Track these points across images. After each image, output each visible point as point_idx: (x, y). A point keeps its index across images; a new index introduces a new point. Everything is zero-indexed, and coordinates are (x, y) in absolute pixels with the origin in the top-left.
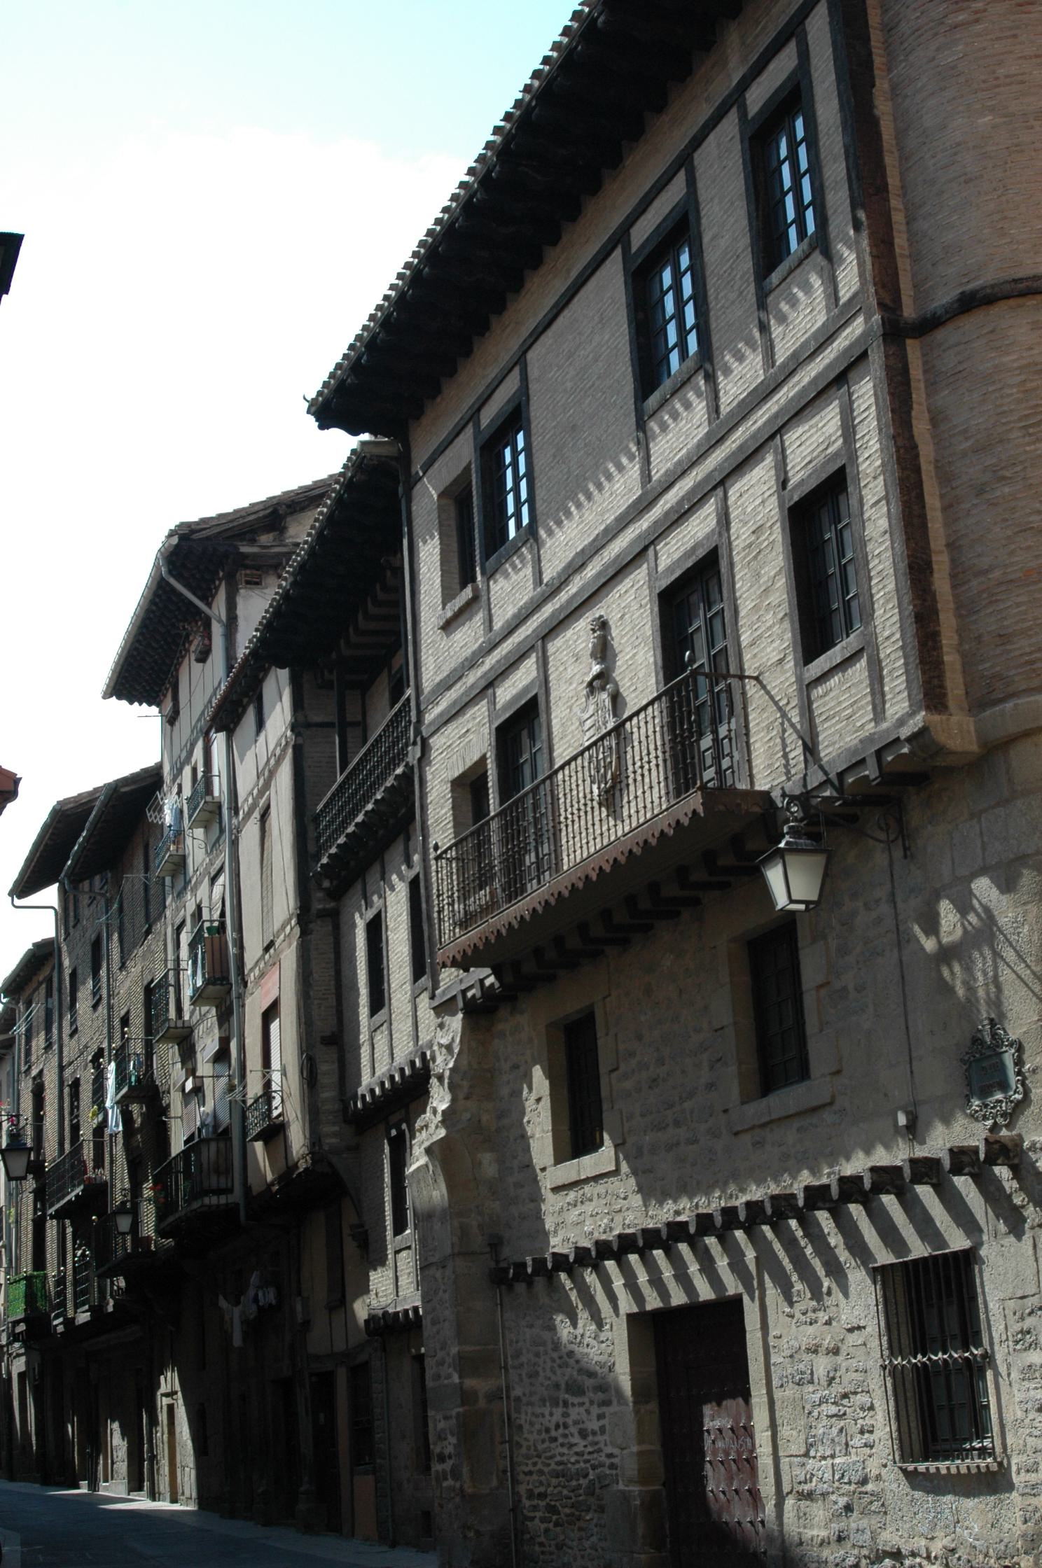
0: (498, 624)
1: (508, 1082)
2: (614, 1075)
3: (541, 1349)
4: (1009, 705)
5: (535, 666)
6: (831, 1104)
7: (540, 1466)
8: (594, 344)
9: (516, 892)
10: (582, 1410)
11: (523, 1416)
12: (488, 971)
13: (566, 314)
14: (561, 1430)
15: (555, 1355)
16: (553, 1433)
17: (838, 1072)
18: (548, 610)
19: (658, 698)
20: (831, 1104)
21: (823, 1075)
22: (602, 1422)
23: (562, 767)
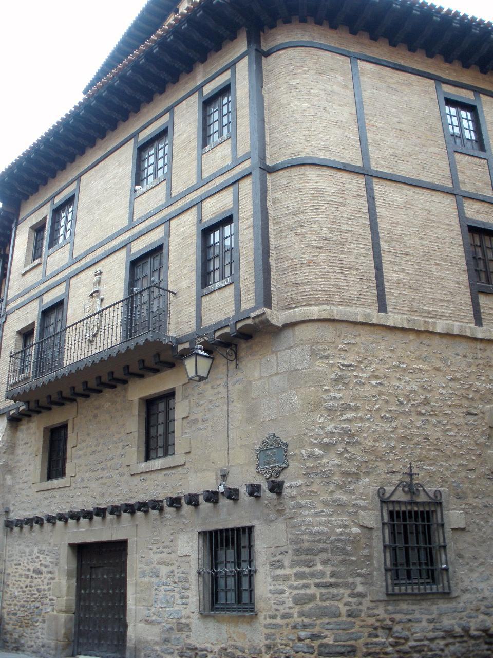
0: (48, 273)
1: (22, 449)
2: (74, 449)
3: (23, 554)
4: (298, 310)
5: (64, 288)
6: (184, 465)
7: (15, 602)
8: (114, 173)
9: (42, 372)
10: (40, 581)
11: (10, 581)
12: (22, 403)
13: (103, 163)
14: (28, 588)
15: (30, 558)
16: (25, 589)
17: (189, 453)
18: (74, 267)
19: (122, 301)
20: (184, 465)
21: (182, 453)
22: (49, 586)
23: (69, 327)
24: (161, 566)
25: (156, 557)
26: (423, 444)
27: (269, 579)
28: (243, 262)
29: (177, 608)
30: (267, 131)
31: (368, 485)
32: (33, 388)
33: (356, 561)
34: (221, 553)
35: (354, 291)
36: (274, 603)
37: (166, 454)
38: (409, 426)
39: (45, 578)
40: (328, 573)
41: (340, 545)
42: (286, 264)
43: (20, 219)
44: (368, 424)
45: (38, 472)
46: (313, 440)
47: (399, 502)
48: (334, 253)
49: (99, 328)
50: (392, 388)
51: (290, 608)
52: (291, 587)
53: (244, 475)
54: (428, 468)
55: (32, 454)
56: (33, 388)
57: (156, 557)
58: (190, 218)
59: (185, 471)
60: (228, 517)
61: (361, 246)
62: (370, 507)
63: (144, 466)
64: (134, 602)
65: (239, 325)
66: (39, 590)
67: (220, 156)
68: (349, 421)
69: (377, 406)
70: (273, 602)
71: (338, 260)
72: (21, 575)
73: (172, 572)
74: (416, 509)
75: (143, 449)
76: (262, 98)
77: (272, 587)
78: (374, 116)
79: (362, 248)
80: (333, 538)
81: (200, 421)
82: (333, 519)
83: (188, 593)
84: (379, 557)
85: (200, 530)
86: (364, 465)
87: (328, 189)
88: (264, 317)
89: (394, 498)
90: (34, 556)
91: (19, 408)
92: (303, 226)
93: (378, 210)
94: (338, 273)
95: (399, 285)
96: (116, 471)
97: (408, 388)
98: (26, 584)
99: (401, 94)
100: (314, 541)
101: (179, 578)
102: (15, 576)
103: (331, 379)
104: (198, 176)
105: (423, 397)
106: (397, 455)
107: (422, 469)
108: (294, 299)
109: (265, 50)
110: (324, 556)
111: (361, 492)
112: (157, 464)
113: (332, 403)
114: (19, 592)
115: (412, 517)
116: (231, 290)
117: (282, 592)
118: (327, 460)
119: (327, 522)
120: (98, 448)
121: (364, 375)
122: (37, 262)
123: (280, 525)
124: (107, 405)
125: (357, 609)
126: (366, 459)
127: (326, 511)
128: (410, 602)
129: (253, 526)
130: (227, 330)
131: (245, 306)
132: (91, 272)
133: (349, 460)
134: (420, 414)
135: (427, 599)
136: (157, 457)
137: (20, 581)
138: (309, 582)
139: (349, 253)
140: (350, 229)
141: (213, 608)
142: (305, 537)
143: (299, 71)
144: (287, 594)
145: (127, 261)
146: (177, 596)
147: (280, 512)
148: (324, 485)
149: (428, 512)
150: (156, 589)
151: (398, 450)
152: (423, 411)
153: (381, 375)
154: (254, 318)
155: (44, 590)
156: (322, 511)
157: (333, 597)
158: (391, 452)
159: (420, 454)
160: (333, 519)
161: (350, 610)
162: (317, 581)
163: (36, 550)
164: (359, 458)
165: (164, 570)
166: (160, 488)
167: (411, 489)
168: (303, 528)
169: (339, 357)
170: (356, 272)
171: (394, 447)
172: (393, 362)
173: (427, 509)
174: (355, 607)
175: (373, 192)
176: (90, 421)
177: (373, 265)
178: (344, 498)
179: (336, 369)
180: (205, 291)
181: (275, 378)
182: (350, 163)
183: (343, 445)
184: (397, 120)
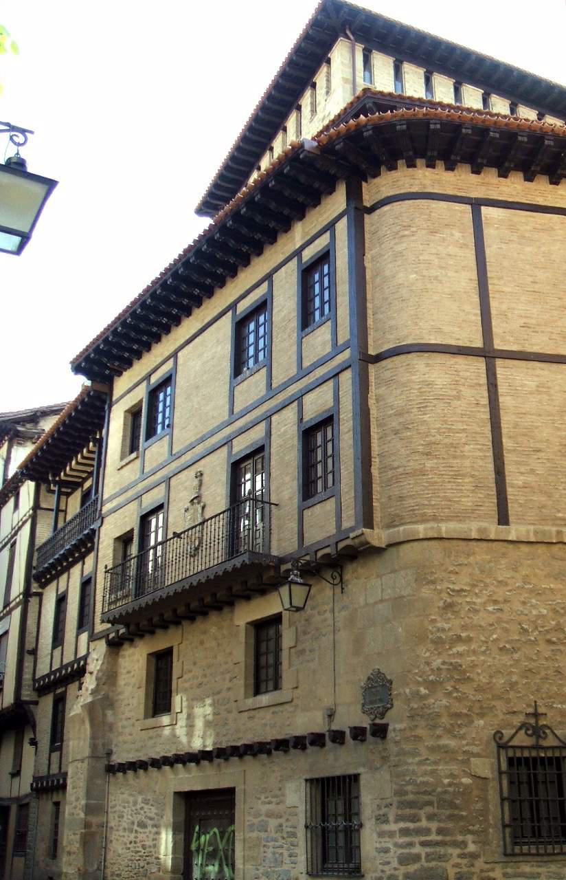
4: (401, 528)
6: (292, 701)
10: (144, 836)
11: (113, 836)
12: (122, 626)
14: (133, 844)
15: (134, 808)
16: (129, 846)
17: (297, 688)
24: (270, 820)
25: (264, 808)
26: (553, 678)
27: (375, 836)
28: (344, 473)
29: (285, 867)
30: (370, 312)
31: (483, 727)
32: (130, 611)
33: (467, 816)
34: (331, 804)
35: (467, 502)
36: (380, 864)
37: (277, 687)
38: (535, 658)
39: (150, 832)
40: (434, 830)
41: (447, 797)
42: (390, 473)
43: (114, 398)
44: (482, 658)
45: (142, 707)
46: (418, 678)
47: (522, 748)
48: (444, 459)
49: (201, 542)
50: (514, 614)
51: (395, 869)
52: (396, 845)
53: (352, 716)
54: (559, 706)
55: (135, 684)
56: (130, 611)
57: (264, 808)
58: (290, 414)
59: (292, 709)
60: (335, 762)
61: (479, 447)
62: (484, 754)
63: (251, 702)
64: (242, 861)
65: (341, 545)
66: (144, 847)
67: (320, 340)
68: (460, 655)
69: (495, 636)
70: (378, 862)
71: (450, 467)
72: (125, 829)
73: (281, 825)
74: (543, 755)
75: (251, 681)
76: (364, 269)
77: (378, 845)
78: (500, 278)
79: (479, 450)
80: (439, 790)
81: (308, 652)
82: (440, 768)
83: (297, 850)
84: (495, 811)
85: (308, 778)
86: (477, 705)
87: (439, 381)
88: (363, 537)
89: (515, 742)
90: (138, 807)
91: (118, 631)
92: (408, 428)
93: (501, 399)
94: (449, 482)
95: (525, 490)
96: (224, 707)
97: (535, 612)
98: (130, 839)
99: (538, 243)
100: (418, 793)
101: (288, 832)
102: (117, 830)
103: (439, 607)
104: (298, 365)
105: (553, 623)
106: (519, 692)
107: (552, 707)
108: (398, 515)
109: (369, 206)
110: (429, 809)
111: (474, 736)
112: (264, 699)
113: (438, 634)
114: (122, 849)
115: (553, 764)
116: (332, 502)
117: (387, 851)
118: (433, 701)
119: (433, 772)
120: (205, 680)
121: (479, 601)
122: (134, 455)
123: (385, 775)
124: (213, 630)
125: (468, 872)
126: (479, 697)
127: (432, 758)
128: (535, 864)
129: (359, 774)
130: (327, 551)
131: (347, 524)
132: (191, 473)
133: (458, 699)
134: (549, 642)
135: (556, 861)
136: (267, 692)
137: (124, 836)
138: (413, 839)
139: (463, 457)
140: (465, 427)
141: (323, 869)
142: (409, 788)
143: (406, 233)
144: (392, 853)
145: (228, 462)
146: (286, 854)
147: (385, 759)
148: (430, 729)
149: (558, 759)
150: (264, 846)
151: (520, 686)
152: (554, 639)
153: (501, 599)
154: (353, 538)
155: (150, 847)
156: (427, 759)
157: (440, 858)
158: (512, 688)
159: (548, 689)
160: (440, 768)
161: (459, 872)
162: (423, 839)
163: (140, 799)
164: (471, 697)
165: (273, 823)
166: (268, 728)
167: (537, 731)
168: (408, 778)
169: (449, 582)
170: (471, 479)
171: (516, 683)
172: (515, 583)
173: (557, 754)
174: (465, 869)
175: (496, 378)
176: (197, 647)
177: (493, 469)
178: (452, 743)
179: (444, 596)
180: (311, 501)
181: (380, 606)
182: (468, 344)
183: (452, 683)
184: (531, 279)
